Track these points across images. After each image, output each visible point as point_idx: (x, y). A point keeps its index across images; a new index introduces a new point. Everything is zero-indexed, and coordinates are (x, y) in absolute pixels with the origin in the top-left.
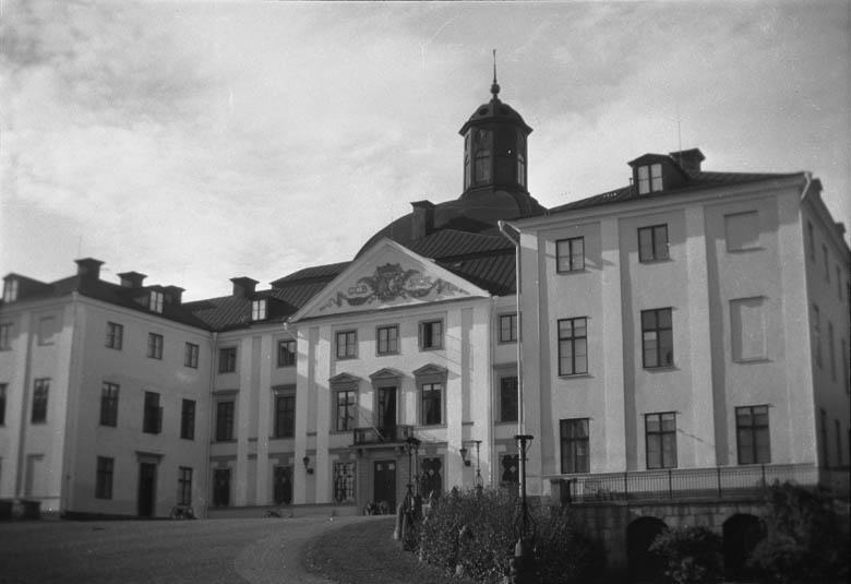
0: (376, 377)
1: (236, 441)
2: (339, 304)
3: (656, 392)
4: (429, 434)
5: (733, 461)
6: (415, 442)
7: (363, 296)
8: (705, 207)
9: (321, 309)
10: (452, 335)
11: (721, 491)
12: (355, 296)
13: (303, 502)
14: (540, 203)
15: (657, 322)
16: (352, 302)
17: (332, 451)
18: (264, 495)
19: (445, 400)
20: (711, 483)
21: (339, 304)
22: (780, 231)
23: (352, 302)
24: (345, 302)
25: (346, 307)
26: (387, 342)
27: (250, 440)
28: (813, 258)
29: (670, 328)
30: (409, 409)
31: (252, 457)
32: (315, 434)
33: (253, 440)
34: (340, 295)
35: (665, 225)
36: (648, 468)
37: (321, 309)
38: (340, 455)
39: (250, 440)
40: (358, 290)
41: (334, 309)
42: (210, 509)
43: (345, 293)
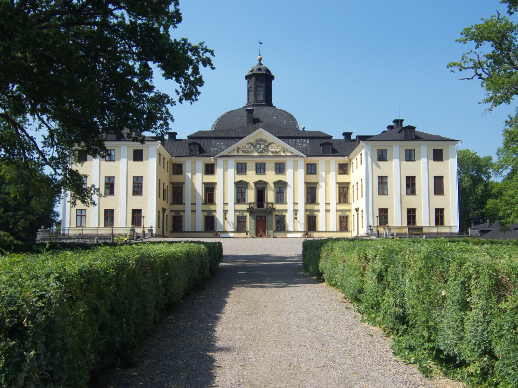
0: (256, 183)
1: (185, 204)
2: (238, 152)
3: (411, 202)
4: (278, 207)
5: (102, 225)
6: (274, 210)
7: (250, 150)
8: (400, 146)
9: (229, 153)
10: (289, 172)
11: (437, 233)
12: (245, 149)
13: (190, 230)
14: (442, 136)
15: (383, 181)
16: (244, 152)
17: (203, 211)
18: (200, 225)
19: (286, 194)
20: (96, 232)
21: (238, 152)
22: (449, 161)
23: (244, 152)
24: (240, 151)
25: (241, 153)
26: (261, 169)
27: (192, 204)
28: (160, 164)
29: (387, 183)
30: (270, 196)
31: (194, 211)
32: (195, 204)
33: (194, 204)
34: (238, 149)
35: (414, 150)
36: (76, 226)
37: (229, 153)
38: (208, 213)
39: (192, 204)
40: (246, 147)
41: (235, 153)
42: (171, 232)
43: (241, 148)
